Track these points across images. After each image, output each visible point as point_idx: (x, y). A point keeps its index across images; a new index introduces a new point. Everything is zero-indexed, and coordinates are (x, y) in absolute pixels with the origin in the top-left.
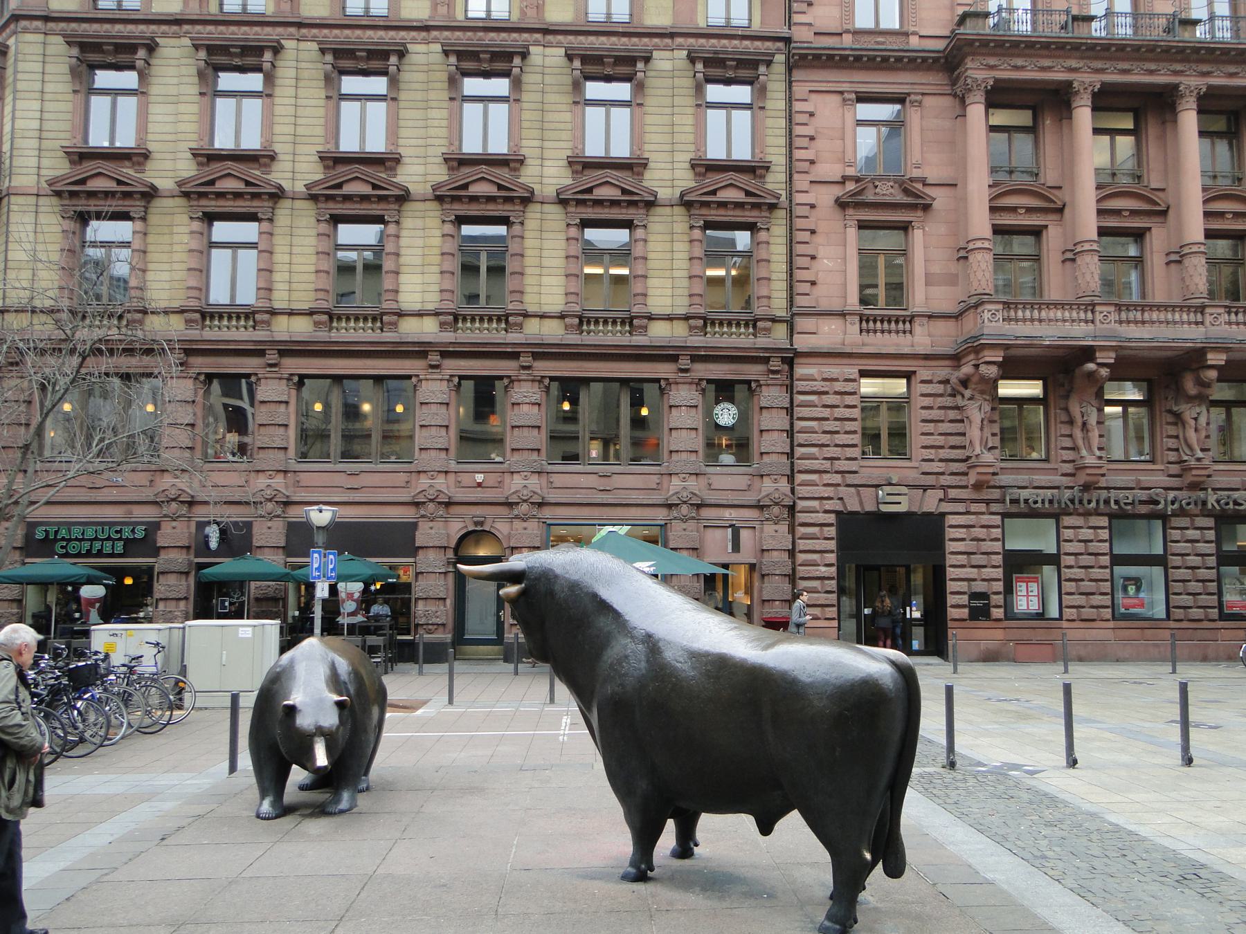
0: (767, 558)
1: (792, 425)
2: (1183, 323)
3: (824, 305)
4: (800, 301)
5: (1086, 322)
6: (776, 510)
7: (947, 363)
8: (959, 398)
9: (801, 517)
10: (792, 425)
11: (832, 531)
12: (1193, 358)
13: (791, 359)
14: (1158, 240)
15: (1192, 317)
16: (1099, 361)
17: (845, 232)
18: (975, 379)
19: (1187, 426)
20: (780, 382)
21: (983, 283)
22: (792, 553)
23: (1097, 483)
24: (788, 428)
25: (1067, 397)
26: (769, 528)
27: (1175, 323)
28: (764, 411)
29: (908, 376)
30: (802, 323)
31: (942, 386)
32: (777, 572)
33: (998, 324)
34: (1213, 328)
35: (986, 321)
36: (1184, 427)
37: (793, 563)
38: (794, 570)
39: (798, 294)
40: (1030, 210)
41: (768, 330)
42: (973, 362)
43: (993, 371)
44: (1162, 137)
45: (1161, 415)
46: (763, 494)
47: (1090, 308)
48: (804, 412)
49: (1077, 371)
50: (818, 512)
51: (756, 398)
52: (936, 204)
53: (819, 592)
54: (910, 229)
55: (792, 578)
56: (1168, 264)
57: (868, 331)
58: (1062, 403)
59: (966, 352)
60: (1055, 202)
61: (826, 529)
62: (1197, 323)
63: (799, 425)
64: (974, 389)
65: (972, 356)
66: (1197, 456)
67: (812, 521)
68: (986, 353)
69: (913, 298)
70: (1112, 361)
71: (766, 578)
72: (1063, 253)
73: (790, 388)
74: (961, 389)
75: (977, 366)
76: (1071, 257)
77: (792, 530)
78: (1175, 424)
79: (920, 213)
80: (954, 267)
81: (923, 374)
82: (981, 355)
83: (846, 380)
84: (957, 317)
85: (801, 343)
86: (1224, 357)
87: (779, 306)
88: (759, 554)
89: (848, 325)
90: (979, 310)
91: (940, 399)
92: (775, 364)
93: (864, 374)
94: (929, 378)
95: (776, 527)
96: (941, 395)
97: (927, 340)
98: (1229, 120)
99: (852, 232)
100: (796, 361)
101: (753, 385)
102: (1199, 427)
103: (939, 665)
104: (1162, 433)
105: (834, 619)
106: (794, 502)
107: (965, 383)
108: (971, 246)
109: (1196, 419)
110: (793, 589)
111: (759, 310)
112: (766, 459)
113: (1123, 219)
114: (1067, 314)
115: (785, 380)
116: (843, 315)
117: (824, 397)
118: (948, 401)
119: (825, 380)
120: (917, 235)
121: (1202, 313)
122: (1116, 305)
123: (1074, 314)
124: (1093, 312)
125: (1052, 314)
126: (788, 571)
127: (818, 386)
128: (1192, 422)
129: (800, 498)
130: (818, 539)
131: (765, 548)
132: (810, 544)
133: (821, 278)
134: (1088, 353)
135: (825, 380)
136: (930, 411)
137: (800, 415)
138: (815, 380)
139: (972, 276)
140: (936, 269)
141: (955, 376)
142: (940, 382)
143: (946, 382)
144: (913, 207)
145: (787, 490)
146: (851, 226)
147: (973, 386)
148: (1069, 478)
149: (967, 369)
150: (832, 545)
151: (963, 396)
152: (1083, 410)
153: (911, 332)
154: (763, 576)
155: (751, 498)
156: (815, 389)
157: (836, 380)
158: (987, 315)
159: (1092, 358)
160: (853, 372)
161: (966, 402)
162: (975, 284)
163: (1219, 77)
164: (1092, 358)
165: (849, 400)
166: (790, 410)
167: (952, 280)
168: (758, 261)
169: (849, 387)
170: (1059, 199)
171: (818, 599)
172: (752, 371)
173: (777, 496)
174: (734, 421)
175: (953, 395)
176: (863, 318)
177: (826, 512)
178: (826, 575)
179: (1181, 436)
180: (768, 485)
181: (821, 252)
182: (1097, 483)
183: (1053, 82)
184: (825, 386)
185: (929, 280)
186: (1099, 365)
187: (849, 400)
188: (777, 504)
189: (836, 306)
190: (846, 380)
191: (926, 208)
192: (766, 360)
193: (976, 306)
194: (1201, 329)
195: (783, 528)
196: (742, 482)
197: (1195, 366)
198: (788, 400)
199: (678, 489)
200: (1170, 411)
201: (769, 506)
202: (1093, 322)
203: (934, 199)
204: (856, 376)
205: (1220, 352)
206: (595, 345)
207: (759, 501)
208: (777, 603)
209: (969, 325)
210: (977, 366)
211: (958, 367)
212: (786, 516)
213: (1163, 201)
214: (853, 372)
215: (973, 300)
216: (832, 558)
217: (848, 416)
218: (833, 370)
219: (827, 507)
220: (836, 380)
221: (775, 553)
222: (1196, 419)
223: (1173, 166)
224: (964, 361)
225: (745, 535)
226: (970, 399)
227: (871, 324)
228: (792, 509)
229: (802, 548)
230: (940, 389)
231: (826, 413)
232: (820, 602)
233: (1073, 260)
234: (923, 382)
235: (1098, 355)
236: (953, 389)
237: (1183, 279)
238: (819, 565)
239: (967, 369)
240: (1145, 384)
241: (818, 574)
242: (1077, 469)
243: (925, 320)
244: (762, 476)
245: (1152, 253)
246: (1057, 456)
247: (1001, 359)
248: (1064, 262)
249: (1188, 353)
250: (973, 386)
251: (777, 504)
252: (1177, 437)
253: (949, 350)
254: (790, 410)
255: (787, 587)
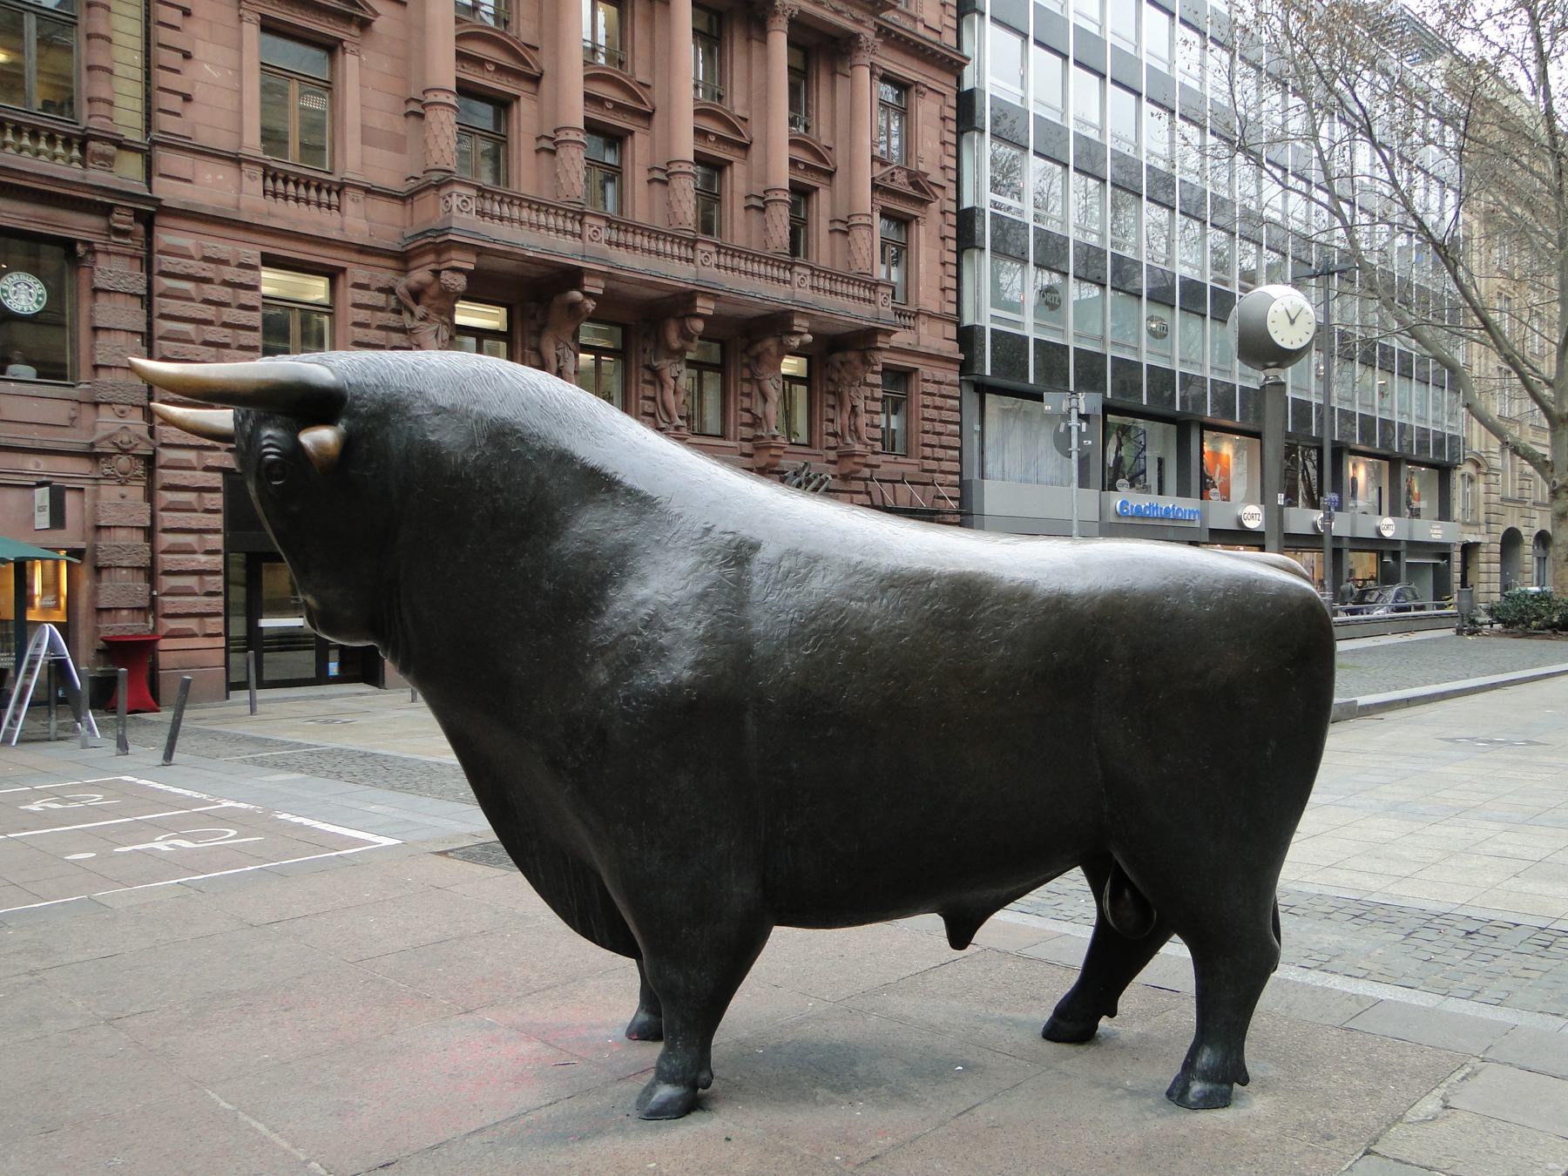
0: (105, 540)
1: (150, 325)
2: (673, 257)
3: (205, 138)
4: (165, 123)
5: (573, 234)
6: (123, 462)
7: (391, 263)
8: (406, 316)
9: (166, 476)
10: (150, 325)
11: (217, 500)
12: (680, 302)
13: (150, 214)
14: (640, 150)
15: (683, 252)
16: (587, 289)
17: (240, 30)
18: (433, 291)
19: (666, 386)
20: (129, 251)
21: (447, 154)
22: (150, 533)
23: (858, 472)
24: (144, 329)
25: (539, 333)
26: (110, 492)
27: (539, 227)
28: (100, 295)
29: (333, 274)
30: (168, 161)
31: (384, 296)
32: (125, 563)
33: (804, 291)
34: (705, 269)
35: (455, 209)
36: (662, 387)
37: (152, 550)
38: (153, 559)
39: (161, 110)
40: (501, 69)
41: (108, 160)
42: (433, 266)
43: (460, 282)
44: (650, 19)
45: (637, 369)
46: (100, 434)
47: (578, 217)
48: (173, 306)
49: (557, 300)
50: (193, 469)
51: (84, 273)
52: (378, 25)
53: (195, 594)
54: (340, 53)
55: (151, 573)
56: (538, 151)
57: (275, 195)
58: (533, 341)
59: (420, 252)
60: (828, 164)
61: (207, 496)
62: (687, 260)
63: (162, 326)
64: (429, 306)
65: (431, 258)
66: (675, 424)
67: (185, 483)
68: (454, 254)
69: (344, 158)
70: (601, 292)
71: (105, 574)
72: (407, 102)
73: (148, 264)
74: (411, 304)
75: (436, 273)
76: (550, 147)
77: (150, 497)
78: (652, 383)
79: (354, 31)
80: (401, 126)
81: (357, 273)
82: (445, 257)
83: (241, 265)
84: (405, 198)
85: (168, 192)
86: (712, 305)
87: (128, 120)
88: (90, 535)
89: (245, 179)
90: (444, 192)
91: (380, 314)
92: (122, 220)
93: (270, 261)
94: (365, 281)
95: (123, 490)
96: (381, 309)
97: (363, 225)
98: (710, 20)
99: (251, 31)
100: (159, 220)
101: (80, 249)
102: (679, 389)
103: (372, 694)
104: (637, 394)
105: (218, 635)
106: (155, 451)
107: (417, 294)
108: (431, 98)
109: (675, 379)
110: (152, 589)
111: (89, 119)
112: (104, 376)
113: (605, 112)
114: (551, 220)
115: (135, 244)
116: (237, 160)
117: (206, 287)
118: (391, 319)
119: (206, 259)
120: (350, 64)
121: (693, 249)
122: (716, 245)
123: (560, 222)
124: (581, 223)
125: (749, 267)
126: (144, 561)
127: (196, 268)
128: (672, 382)
129: (164, 445)
130: (195, 511)
131: (102, 523)
132: (179, 519)
133: (198, 92)
134: (572, 276)
135: (206, 259)
136: (367, 331)
137: (165, 311)
138: (191, 258)
139: (431, 141)
140: (376, 121)
141: (401, 285)
142: (380, 290)
143: (389, 291)
144: (347, 18)
145: (143, 429)
146: (249, 21)
147: (430, 302)
148: (747, 459)
149: (420, 275)
150: (217, 521)
151: (412, 314)
152: (560, 353)
153: (914, 328)
154: (98, 570)
155: (76, 439)
156: (191, 271)
157: (225, 262)
158: (455, 201)
159: (578, 286)
160: (253, 254)
161: (417, 324)
162: (436, 155)
163: (848, 19)
164: (578, 286)
165: (246, 297)
166: (147, 300)
167: (398, 144)
168: (89, 37)
169: (246, 277)
170: (537, 64)
171: (194, 605)
172: (80, 226)
173: (126, 439)
174: (38, 308)
175: (399, 312)
176: (270, 174)
177: (208, 469)
178: (208, 567)
179: (658, 399)
180: (107, 422)
181: (199, 51)
182: (858, 472)
183: (838, 28)
184: (209, 271)
185: (367, 137)
186: (588, 295)
187: (246, 297)
188: (125, 452)
189: (225, 143)
190: (241, 265)
191: (365, 25)
192: (105, 210)
193: (439, 186)
194: (692, 267)
195: (136, 492)
196: (58, 411)
197: (681, 313)
198: (144, 282)
199: (115, 428)
200: (649, 367)
201: (109, 455)
202: (580, 236)
203: (377, 14)
204: (257, 261)
205: (710, 299)
206: (41, 176)
207: (92, 445)
208: (125, 613)
209: (428, 211)
210: (436, 273)
211: (405, 271)
212: (140, 472)
213: (650, 102)
214: (253, 254)
215: (436, 177)
216: (217, 541)
217: (244, 322)
218: (222, 246)
219: (211, 462)
220: (225, 262)
221: (122, 533)
222: (675, 379)
223: (663, 59)
224: (414, 264)
225: (70, 499)
226: (422, 319)
227: (324, 195)
228: (150, 461)
229: (168, 525)
230: (380, 299)
231: (209, 312)
232: (197, 610)
233: (421, 116)
234: (357, 286)
235: (586, 280)
236: (399, 302)
237: (669, 204)
238: (194, 552)
239: (420, 275)
240: (618, 331)
241: (193, 566)
242: (839, 456)
243: (360, 195)
244: (96, 404)
245: (633, 165)
246: (735, 432)
247: (472, 267)
248: (650, 182)
249: (675, 295)
250: (430, 302)
251: (125, 452)
252: (653, 399)
253: (393, 244)
254: (147, 300)
255: (141, 586)
